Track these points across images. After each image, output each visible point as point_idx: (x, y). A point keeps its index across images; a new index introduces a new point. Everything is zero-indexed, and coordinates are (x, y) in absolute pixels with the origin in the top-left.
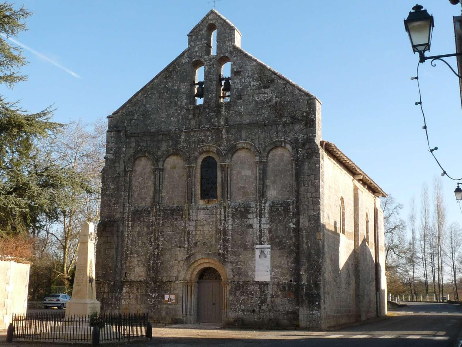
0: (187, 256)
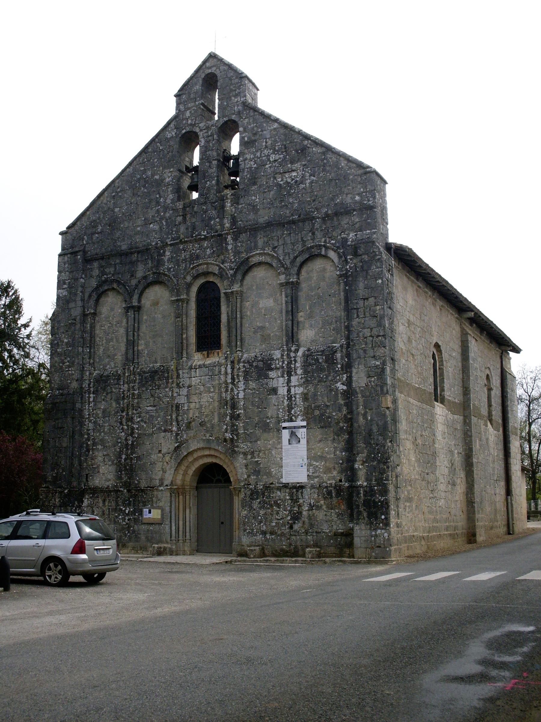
0: (176, 445)
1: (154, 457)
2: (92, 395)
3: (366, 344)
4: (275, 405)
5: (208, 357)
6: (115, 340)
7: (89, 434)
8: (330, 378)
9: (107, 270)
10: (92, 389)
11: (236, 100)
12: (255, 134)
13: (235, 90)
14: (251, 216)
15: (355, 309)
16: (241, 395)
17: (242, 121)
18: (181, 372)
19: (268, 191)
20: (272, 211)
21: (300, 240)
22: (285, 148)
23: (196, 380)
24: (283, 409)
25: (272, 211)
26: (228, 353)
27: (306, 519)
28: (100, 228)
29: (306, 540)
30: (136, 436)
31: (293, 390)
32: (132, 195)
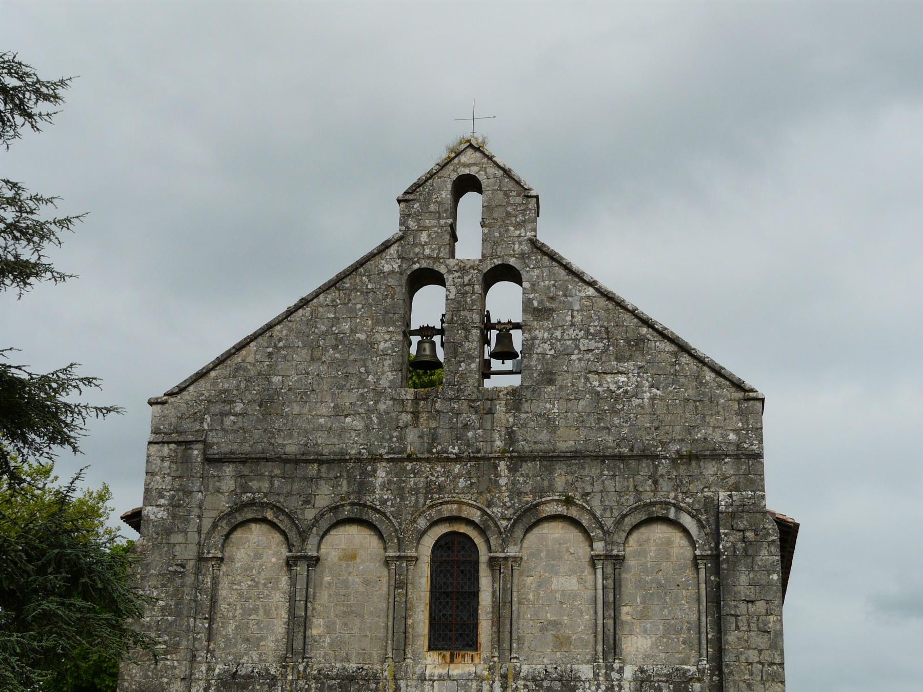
3: (751, 675)
5: (452, 661)
6: (261, 612)
9: (254, 485)
11: (518, 232)
12: (552, 299)
13: (516, 216)
14: (544, 436)
15: (732, 615)
17: (527, 272)
19: (576, 399)
20: (583, 433)
21: (631, 488)
22: (608, 333)
25: (583, 433)
26: (496, 659)
28: (239, 408)
32: (309, 358)
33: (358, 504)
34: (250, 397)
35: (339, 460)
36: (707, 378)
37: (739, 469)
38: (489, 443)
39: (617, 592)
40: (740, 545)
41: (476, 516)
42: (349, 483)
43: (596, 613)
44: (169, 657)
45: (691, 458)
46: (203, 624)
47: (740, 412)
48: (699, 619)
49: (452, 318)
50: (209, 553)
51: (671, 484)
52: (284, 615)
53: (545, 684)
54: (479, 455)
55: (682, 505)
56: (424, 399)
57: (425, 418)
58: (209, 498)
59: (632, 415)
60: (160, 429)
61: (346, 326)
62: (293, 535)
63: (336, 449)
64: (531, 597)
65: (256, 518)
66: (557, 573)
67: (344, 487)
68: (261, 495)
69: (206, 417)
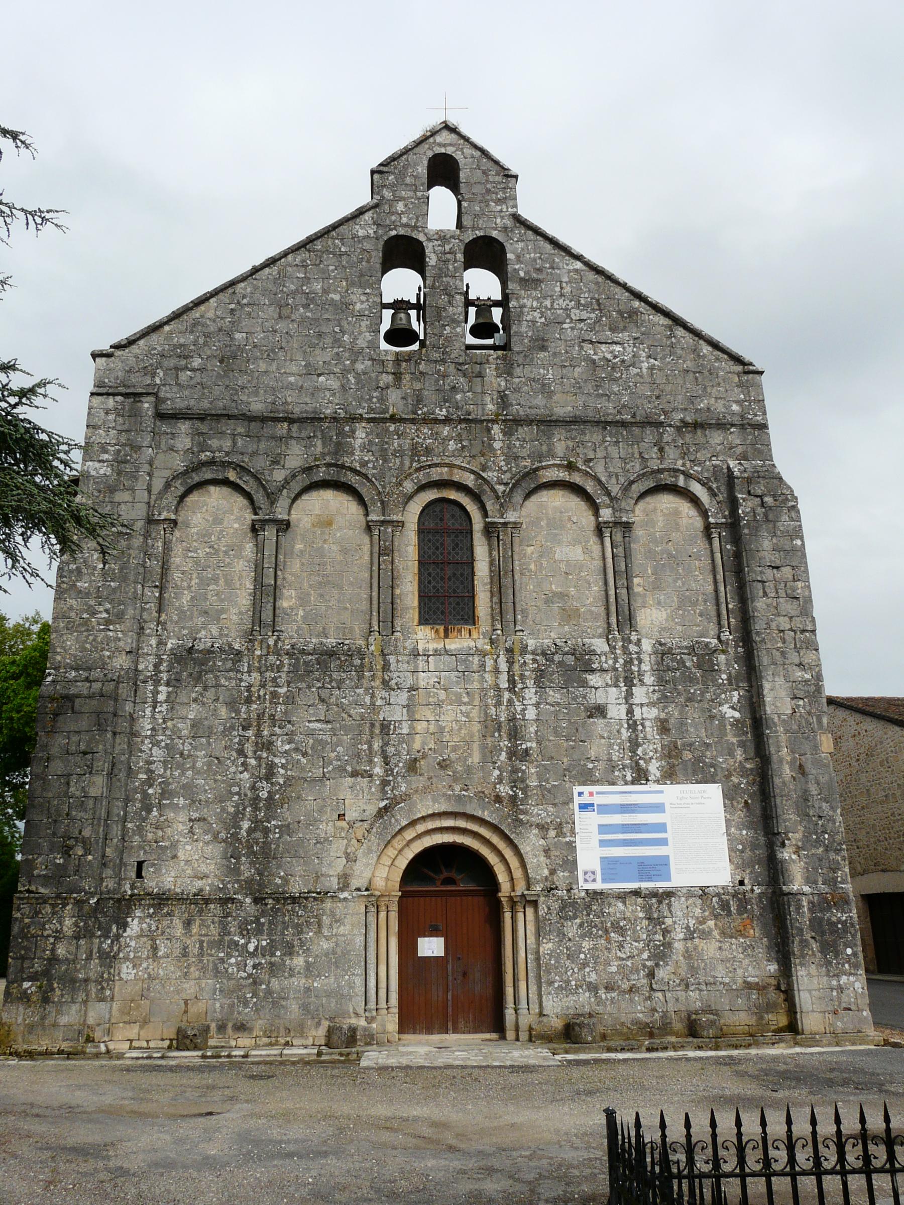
0: (382, 804)
1: (326, 828)
2: (162, 688)
3: (784, 643)
4: (603, 738)
5: (446, 636)
7: (152, 772)
8: (708, 696)
9: (214, 443)
10: (164, 676)
11: (499, 208)
12: (539, 270)
13: (496, 194)
14: (539, 400)
15: (759, 581)
16: (531, 714)
18: (392, 659)
19: (571, 366)
21: (637, 455)
22: (599, 304)
23: (429, 678)
24: (619, 745)
27: (681, 958)
28: (196, 362)
29: (687, 998)
30: (281, 781)
31: (637, 711)
32: (276, 316)
33: (336, 465)
34: (209, 353)
35: (312, 419)
36: (705, 351)
37: (745, 439)
38: (480, 407)
39: (628, 561)
40: (760, 510)
41: (469, 480)
42: (324, 443)
43: (606, 583)
44: (111, 627)
45: (696, 426)
46: (152, 592)
47: (740, 385)
48: (716, 591)
49: (434, 283)
50: (160, 514)
51: (679, 451)
52: (250, 586)
53: (557, 658)
54: (470, 417)
55: (692, 472)
56: (406, 361)
57: (408, 379)
58: (161, 456)
59: (631, 384)
60: (104, 382)
61: (318, 287)
62: (259, 497)
63: (309, 408)
64: (532, 567)
65: (216, 479)
66: (559, 542)
67: (319, 447)
68: (222, 454)
69: (158, 371)
